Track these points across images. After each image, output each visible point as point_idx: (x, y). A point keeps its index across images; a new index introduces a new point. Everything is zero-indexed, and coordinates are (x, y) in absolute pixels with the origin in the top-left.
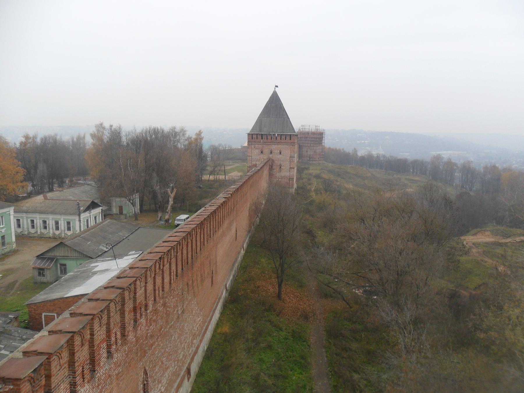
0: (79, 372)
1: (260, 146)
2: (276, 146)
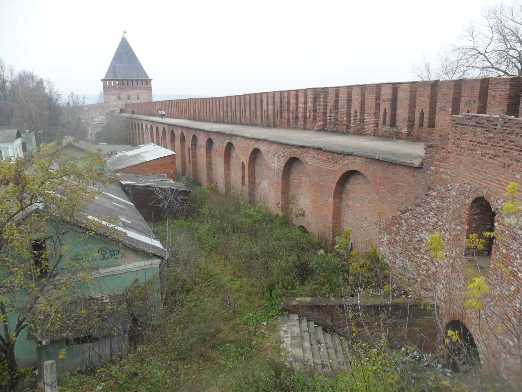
0: (291, 111)
1: (117, 92)
2: (133, 91)
